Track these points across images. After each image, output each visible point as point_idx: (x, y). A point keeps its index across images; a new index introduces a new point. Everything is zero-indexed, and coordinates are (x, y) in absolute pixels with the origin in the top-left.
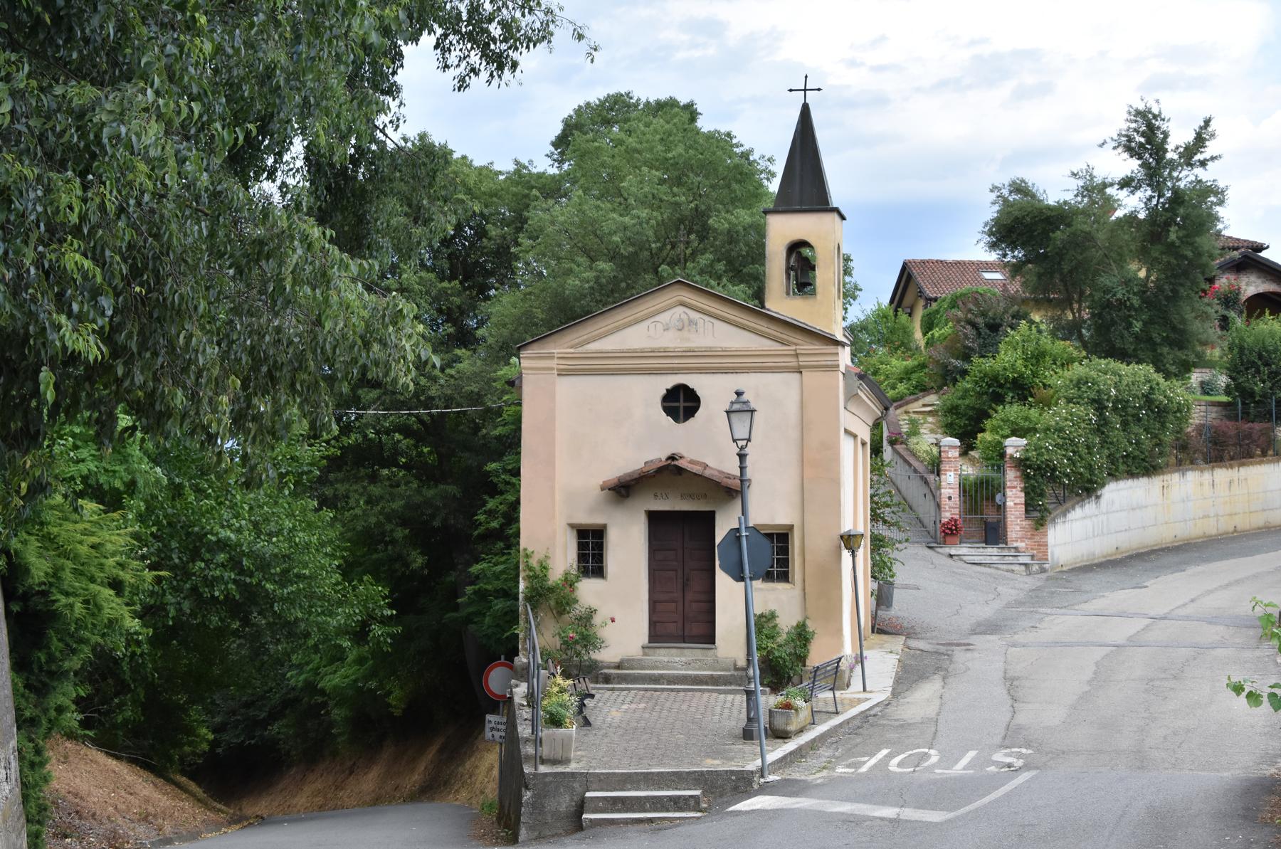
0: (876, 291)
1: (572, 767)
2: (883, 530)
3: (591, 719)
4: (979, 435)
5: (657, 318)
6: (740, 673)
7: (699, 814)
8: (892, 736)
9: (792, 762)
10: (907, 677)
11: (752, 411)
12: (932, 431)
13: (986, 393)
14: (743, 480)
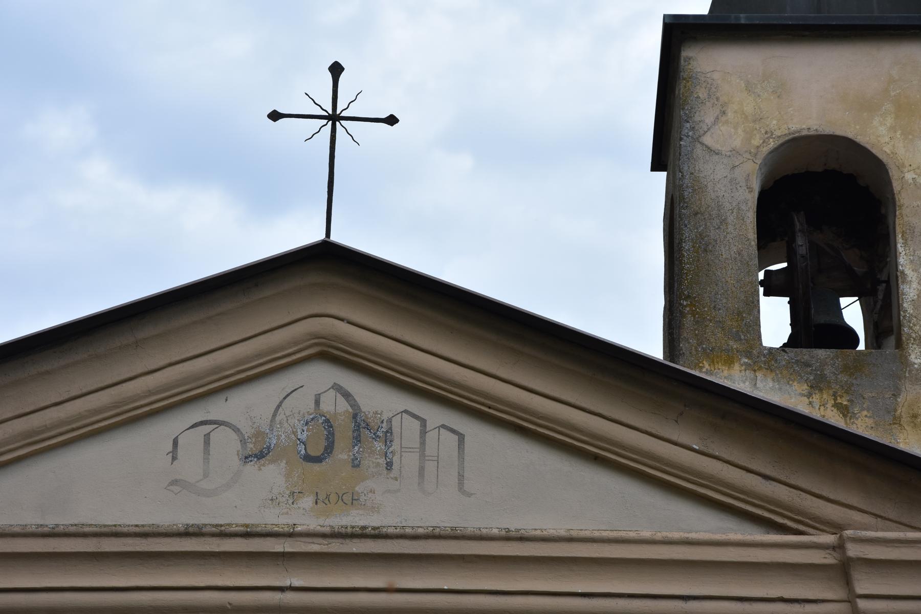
5: (216, 409)
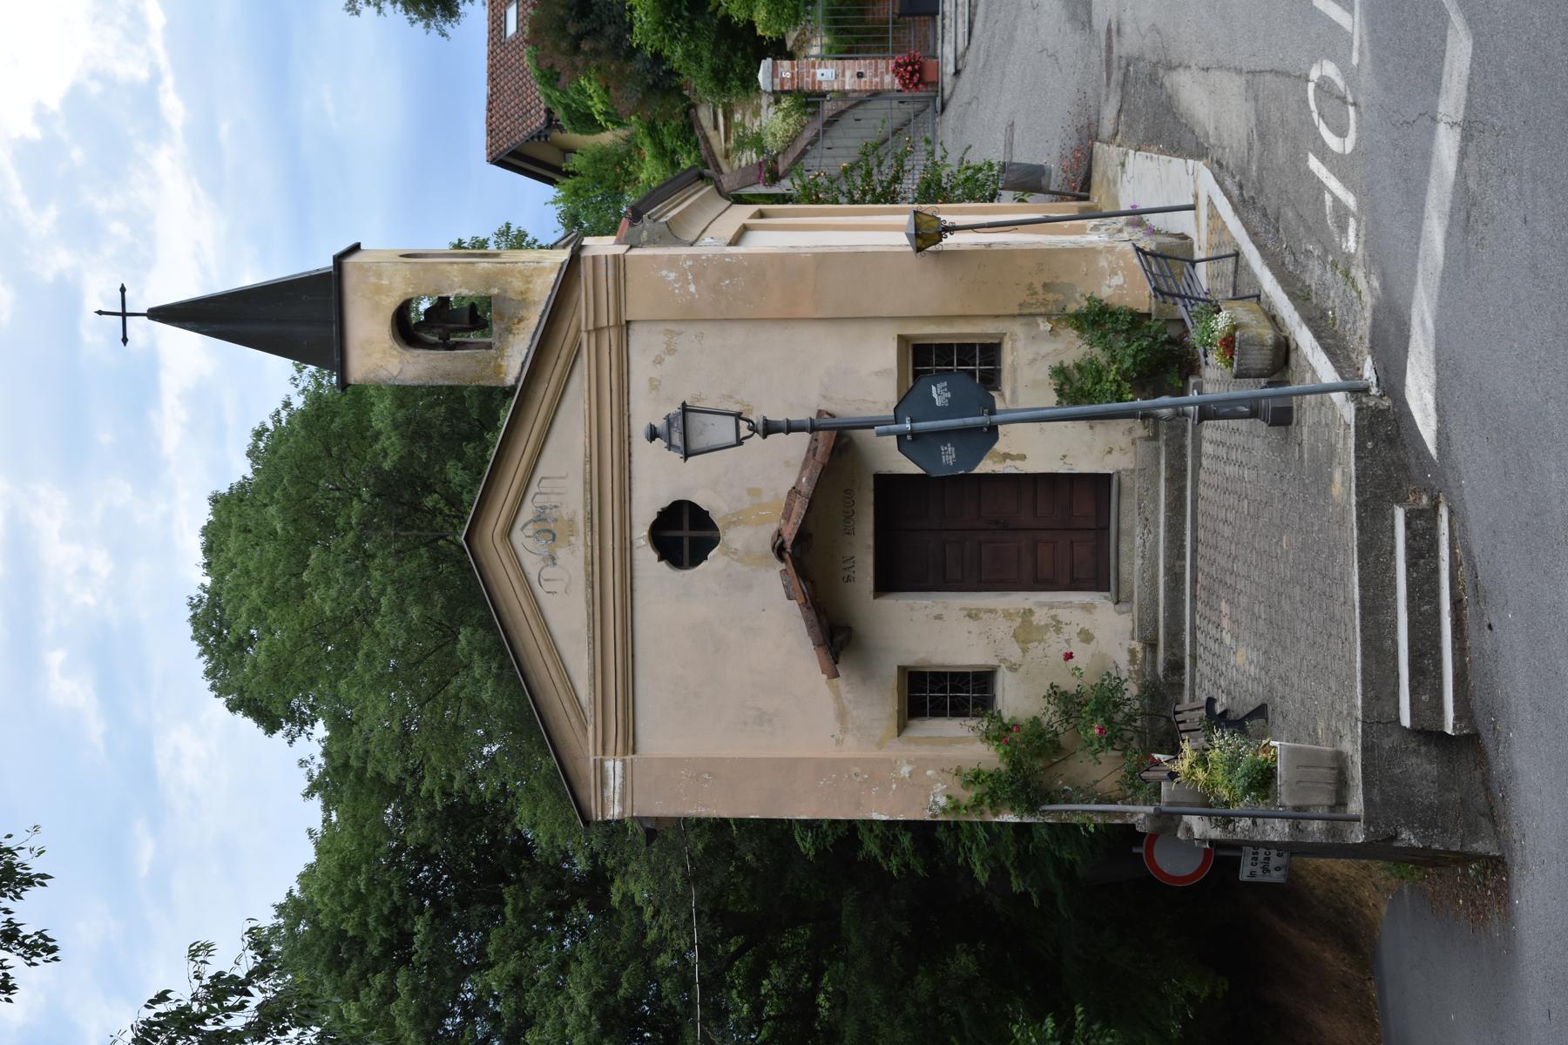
0: (535, 205)
1: (1352, 748)
2: (910, 184)
3: (1253, 703)
4: (759, 32)
5: (533, 578)
6: (1163, 429)
7: (1444, 512)
8: (1281, 151)
9: (1334, 335)
10: (1169, 133)
11: (685, 409)
12: (756, 113)
13: (691, 22)
14: (813, 428)
